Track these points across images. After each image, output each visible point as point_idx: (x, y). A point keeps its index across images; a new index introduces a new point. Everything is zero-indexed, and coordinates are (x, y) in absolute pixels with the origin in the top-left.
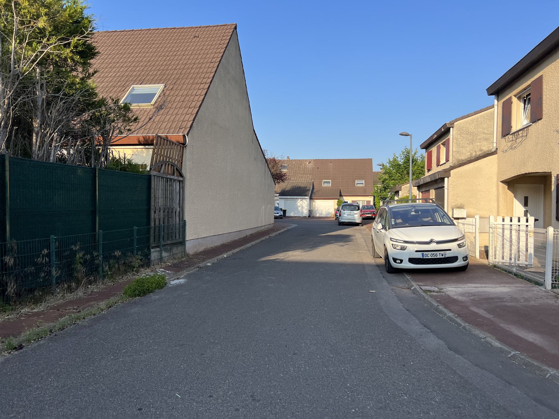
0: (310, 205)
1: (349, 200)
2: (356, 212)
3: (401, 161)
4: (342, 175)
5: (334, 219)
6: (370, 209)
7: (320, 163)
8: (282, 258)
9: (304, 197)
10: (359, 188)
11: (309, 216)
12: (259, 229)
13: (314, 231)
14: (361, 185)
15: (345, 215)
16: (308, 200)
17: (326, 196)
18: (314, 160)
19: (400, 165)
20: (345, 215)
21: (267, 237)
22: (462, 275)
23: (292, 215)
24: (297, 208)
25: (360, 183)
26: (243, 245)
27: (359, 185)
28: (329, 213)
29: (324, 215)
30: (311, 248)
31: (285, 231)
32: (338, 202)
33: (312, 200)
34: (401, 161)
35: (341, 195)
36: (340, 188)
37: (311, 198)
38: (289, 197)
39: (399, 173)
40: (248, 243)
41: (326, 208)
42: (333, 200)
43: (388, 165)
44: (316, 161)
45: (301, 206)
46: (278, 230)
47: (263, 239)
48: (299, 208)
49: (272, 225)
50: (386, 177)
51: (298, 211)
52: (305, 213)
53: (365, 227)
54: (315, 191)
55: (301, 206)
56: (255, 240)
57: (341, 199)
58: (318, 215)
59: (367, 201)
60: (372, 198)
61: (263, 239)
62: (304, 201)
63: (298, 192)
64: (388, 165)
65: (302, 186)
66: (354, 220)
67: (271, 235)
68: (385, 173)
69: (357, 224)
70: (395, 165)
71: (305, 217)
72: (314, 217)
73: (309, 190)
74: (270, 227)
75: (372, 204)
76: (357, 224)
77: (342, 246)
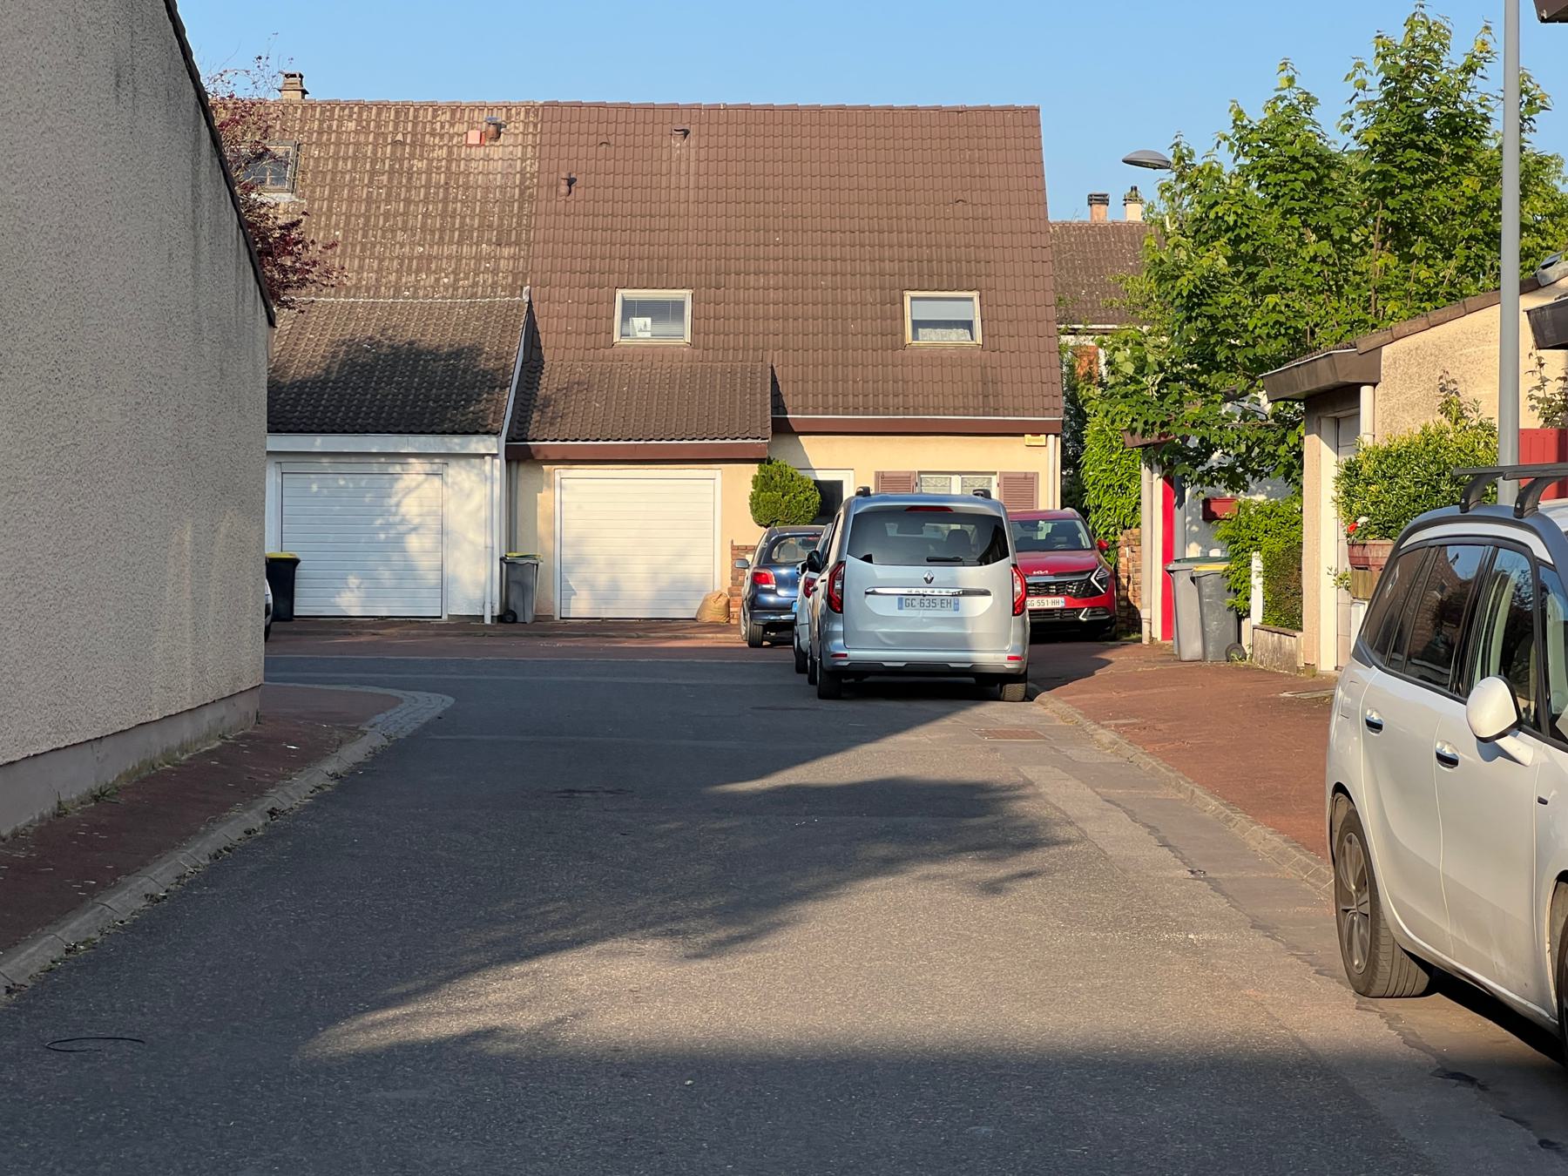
0: (513, 513)
1: (848, 464)
2: (973, 575)
3: (1340, 129)
4: (784, 257)
5: (737, 638)
6: (1047, 545)
7: (590, 145)
8: (526, 1020)
9: (455, 443)
10: (938, 360)
11: (507, 616)
12: (155, 745)
13: (746, 755)
14: (956, 337)
15: (883, 607)
16: (497, 468)
17: (656, 430)
18: (530, 108)
19: (1327, 162)
20: (883, 607)
21: (254, 818)
22: (1451, 1069)
23: (350, 603)
24: (398, 543)
25: (943, 322)
26: (68, 906)
27: (929, 337)
28: (683, 587)
29: (637, 601)
30: (725, 915)
31: (377, 756)
32: (762, 484)
33: (524, 473)
34: (1340, 129)
35: (782, 428)
36: (774, 357)
37: (520, 456)
38: (319, 443)
39: (1324, 233)
40: (108, 880)
41: (655, 539)
42: (716, 472)
43: (1228, 162)
44: (554, 120)
45: (429, 529)
46: (312, 753)
47: (228, 832)
48: (414, 543)
49: (248, 706)
50: (1217, 259)
51: (408, 571)
52: (473, 585)
53: (1050, 707)
54: (548, 384)
55: (429, 529)
56: (158, 851)
57: (784, 456)
58: (581, 607)
59: (1009, 480)
60: (1052, 445)
61: (228, 832)
62: (459, 474)
63: (396, 395)
64: (1228, 162)
65: (431, 338)
66: (963, 642)
67: (276, 798)
68: (1203, 232)
69: (980, 686)
70: (1285, 158)
71: (467, 625)
72: (549, 627)
73: (495, 382)
74: (237, 718)
75: (1048, 498)
76: (980, 686)
77: (993, 888)
